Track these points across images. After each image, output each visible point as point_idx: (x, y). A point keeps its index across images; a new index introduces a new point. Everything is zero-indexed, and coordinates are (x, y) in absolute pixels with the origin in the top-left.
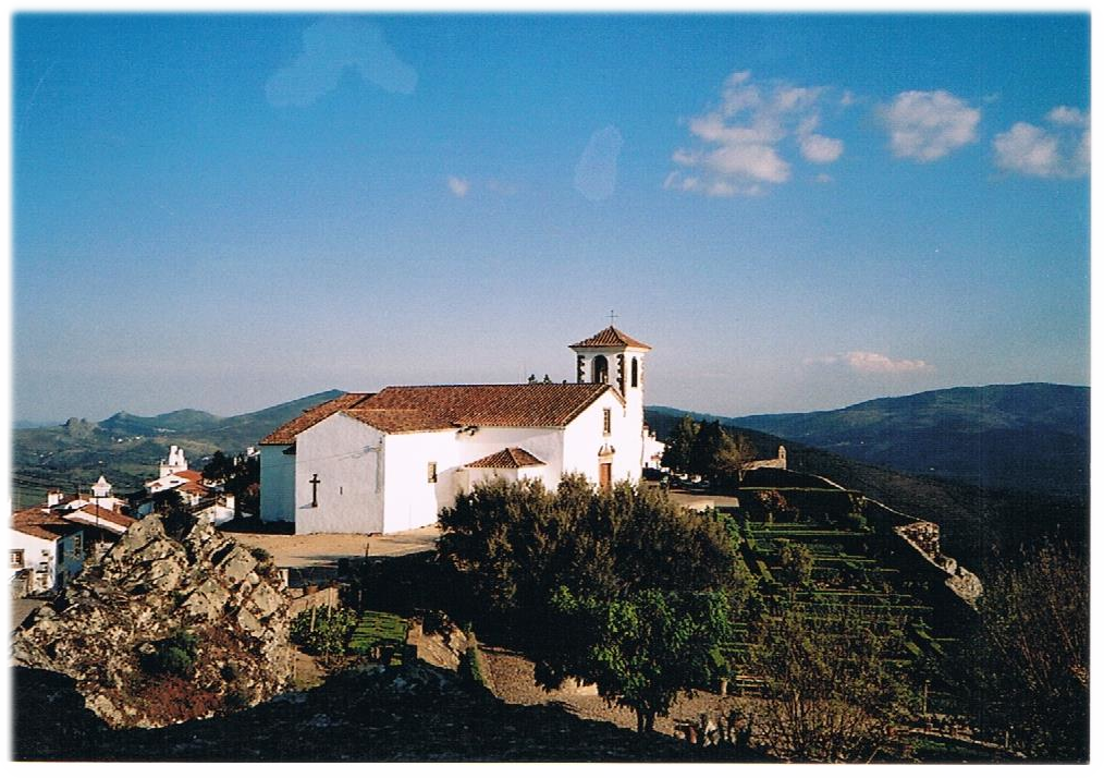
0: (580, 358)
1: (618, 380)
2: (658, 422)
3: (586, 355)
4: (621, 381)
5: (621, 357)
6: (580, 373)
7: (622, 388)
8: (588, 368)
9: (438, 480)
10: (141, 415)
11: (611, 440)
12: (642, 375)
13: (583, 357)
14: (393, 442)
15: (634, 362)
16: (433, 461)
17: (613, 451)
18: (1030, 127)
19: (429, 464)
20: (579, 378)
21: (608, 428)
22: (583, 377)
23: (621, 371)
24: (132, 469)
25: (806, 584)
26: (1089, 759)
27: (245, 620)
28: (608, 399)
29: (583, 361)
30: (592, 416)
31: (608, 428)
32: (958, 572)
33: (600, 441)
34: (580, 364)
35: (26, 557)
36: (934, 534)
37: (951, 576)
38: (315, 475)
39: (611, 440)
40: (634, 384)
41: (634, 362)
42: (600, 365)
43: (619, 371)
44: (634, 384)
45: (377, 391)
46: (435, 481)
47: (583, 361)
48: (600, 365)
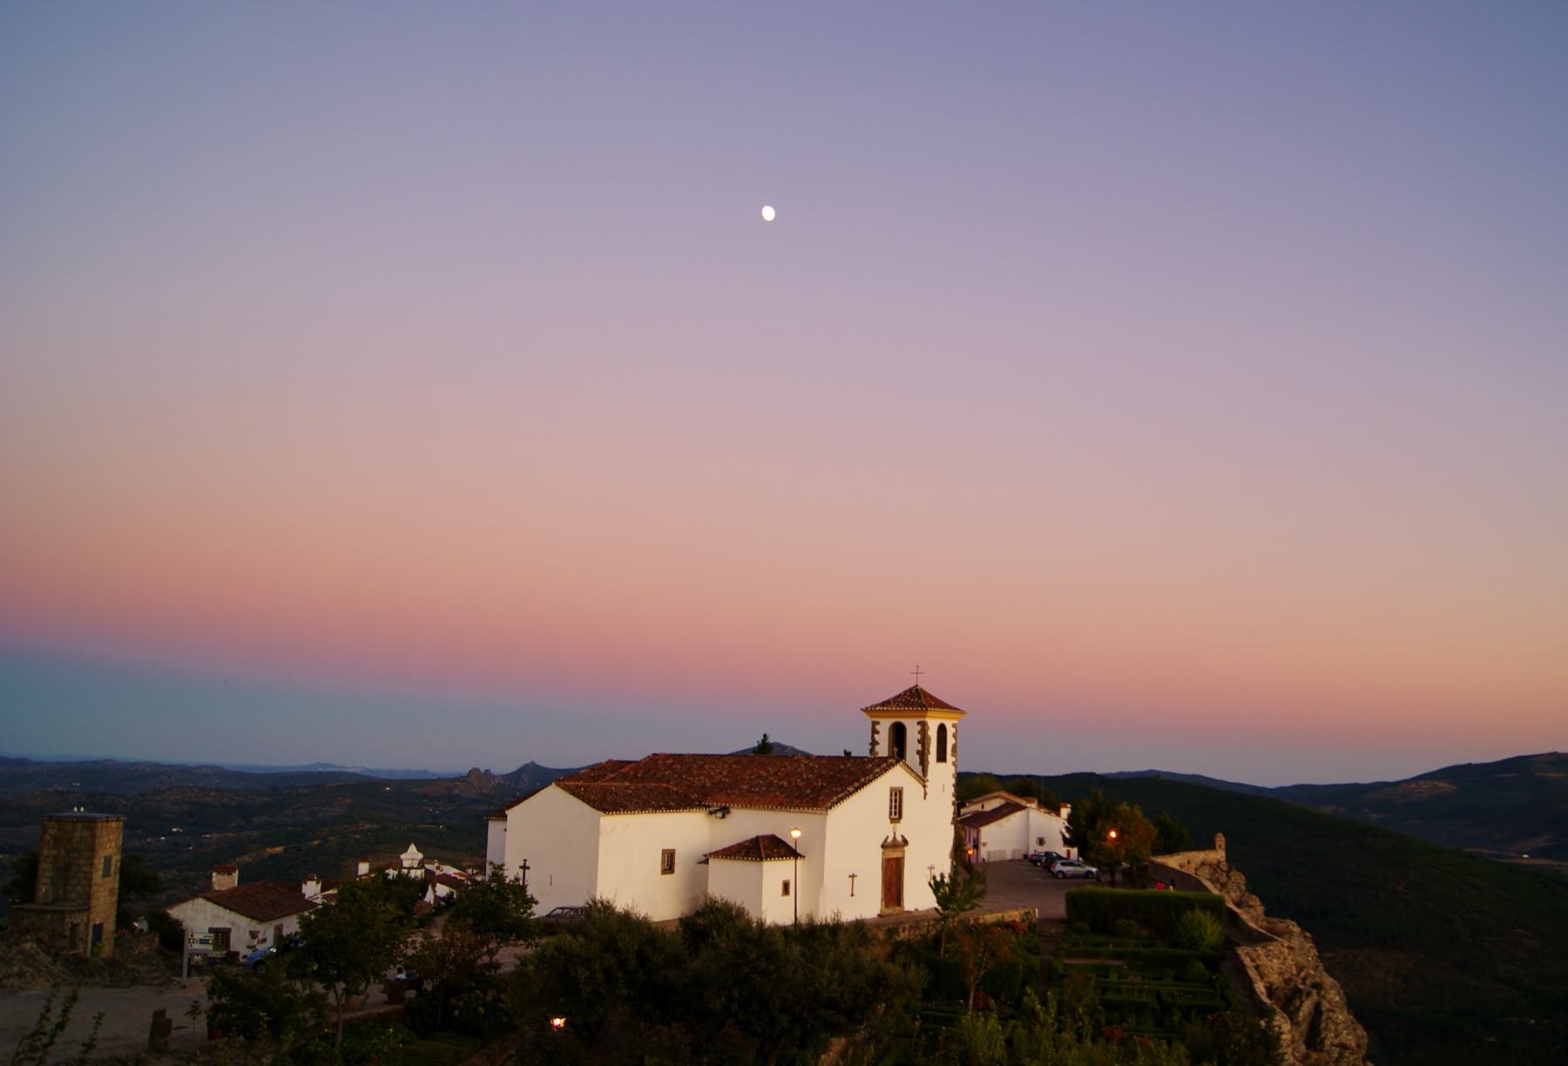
0: (875, 724)
3: (905, 721)
4: (923, 755)
5: (924, 725)
6: (874, 743)
7: (924, 762)
8: (883, 738)
9: (148, 1018)
11: (902, 829)
12: (954, 747)
14: (613, 824)
15: (942, 729)
17: (905, 842)
18: (769, 922)
19: (664, 852)
20: (872, 751)
21: (896, 813)
23: (924, 741)
26: (957, 786)
28: (897, 776)
30: (871, 798)
31: (896, 813)
33: (886, 830)
34: (875, 732)
35: (233, 937)
39: (902, 829)
40: (941, 758)
41: (942, 729)
42: (898, 733)
44: (941, 758)
45: (638, 758)
48: (898, 733)
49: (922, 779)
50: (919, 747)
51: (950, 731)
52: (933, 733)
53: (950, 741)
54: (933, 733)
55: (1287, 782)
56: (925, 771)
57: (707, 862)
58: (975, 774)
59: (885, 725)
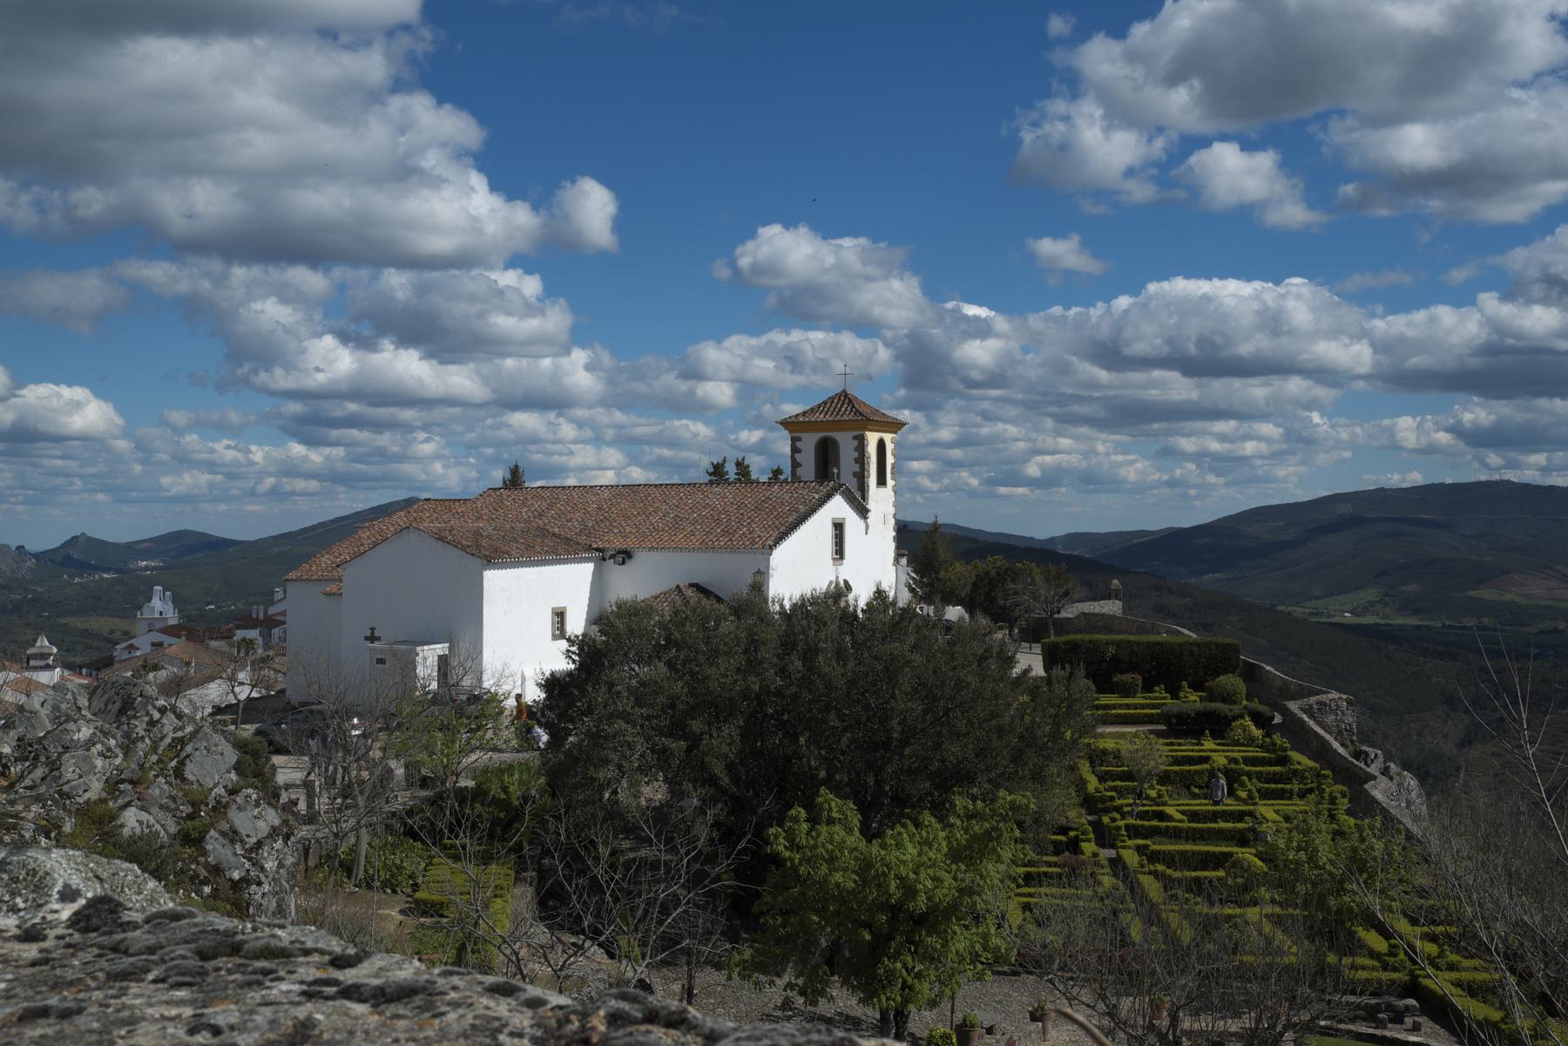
1: (855, 474)
2: (915, 542)
4: (861, 477)
5: (861, 441)
10: (988, 530)
13: (799, 439)
15: (881, 445)
16: (558, 604)
21: (839, 551)
22: (799, 471)
23: (861, 459)
24: (102, 624)
25: (1153, 793)
27: (215, 846)
28: (837, 507)
29: (798, 444)
31: (839, 551)
32: (1385, 771)
36: (636, 796)
37: (1375, 778)
38: (373, 629)
40: (882, 481)
41: (881, 445)
43: (856, 461)
44: (882, 481)
46: (367, 638)
47: (798, 444)
49: (863, 512)
50: (856, 468)
51: (889, 447)
52: (872, 450)
53: (890, 460)
54: (872, 450)
55: (994, 530)
56: (864, 497)
57: (760, 865)
58: (224, 544)
59: (809, 441)
